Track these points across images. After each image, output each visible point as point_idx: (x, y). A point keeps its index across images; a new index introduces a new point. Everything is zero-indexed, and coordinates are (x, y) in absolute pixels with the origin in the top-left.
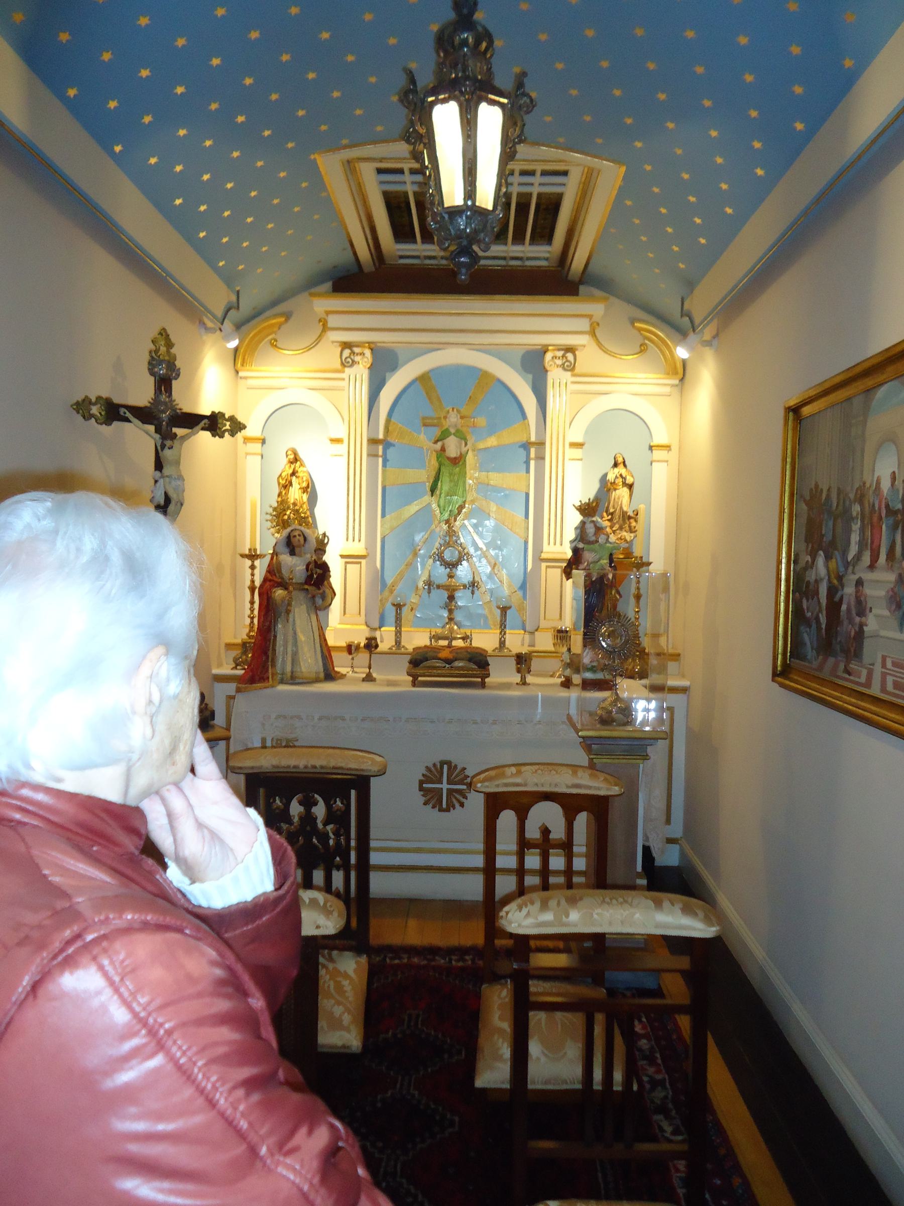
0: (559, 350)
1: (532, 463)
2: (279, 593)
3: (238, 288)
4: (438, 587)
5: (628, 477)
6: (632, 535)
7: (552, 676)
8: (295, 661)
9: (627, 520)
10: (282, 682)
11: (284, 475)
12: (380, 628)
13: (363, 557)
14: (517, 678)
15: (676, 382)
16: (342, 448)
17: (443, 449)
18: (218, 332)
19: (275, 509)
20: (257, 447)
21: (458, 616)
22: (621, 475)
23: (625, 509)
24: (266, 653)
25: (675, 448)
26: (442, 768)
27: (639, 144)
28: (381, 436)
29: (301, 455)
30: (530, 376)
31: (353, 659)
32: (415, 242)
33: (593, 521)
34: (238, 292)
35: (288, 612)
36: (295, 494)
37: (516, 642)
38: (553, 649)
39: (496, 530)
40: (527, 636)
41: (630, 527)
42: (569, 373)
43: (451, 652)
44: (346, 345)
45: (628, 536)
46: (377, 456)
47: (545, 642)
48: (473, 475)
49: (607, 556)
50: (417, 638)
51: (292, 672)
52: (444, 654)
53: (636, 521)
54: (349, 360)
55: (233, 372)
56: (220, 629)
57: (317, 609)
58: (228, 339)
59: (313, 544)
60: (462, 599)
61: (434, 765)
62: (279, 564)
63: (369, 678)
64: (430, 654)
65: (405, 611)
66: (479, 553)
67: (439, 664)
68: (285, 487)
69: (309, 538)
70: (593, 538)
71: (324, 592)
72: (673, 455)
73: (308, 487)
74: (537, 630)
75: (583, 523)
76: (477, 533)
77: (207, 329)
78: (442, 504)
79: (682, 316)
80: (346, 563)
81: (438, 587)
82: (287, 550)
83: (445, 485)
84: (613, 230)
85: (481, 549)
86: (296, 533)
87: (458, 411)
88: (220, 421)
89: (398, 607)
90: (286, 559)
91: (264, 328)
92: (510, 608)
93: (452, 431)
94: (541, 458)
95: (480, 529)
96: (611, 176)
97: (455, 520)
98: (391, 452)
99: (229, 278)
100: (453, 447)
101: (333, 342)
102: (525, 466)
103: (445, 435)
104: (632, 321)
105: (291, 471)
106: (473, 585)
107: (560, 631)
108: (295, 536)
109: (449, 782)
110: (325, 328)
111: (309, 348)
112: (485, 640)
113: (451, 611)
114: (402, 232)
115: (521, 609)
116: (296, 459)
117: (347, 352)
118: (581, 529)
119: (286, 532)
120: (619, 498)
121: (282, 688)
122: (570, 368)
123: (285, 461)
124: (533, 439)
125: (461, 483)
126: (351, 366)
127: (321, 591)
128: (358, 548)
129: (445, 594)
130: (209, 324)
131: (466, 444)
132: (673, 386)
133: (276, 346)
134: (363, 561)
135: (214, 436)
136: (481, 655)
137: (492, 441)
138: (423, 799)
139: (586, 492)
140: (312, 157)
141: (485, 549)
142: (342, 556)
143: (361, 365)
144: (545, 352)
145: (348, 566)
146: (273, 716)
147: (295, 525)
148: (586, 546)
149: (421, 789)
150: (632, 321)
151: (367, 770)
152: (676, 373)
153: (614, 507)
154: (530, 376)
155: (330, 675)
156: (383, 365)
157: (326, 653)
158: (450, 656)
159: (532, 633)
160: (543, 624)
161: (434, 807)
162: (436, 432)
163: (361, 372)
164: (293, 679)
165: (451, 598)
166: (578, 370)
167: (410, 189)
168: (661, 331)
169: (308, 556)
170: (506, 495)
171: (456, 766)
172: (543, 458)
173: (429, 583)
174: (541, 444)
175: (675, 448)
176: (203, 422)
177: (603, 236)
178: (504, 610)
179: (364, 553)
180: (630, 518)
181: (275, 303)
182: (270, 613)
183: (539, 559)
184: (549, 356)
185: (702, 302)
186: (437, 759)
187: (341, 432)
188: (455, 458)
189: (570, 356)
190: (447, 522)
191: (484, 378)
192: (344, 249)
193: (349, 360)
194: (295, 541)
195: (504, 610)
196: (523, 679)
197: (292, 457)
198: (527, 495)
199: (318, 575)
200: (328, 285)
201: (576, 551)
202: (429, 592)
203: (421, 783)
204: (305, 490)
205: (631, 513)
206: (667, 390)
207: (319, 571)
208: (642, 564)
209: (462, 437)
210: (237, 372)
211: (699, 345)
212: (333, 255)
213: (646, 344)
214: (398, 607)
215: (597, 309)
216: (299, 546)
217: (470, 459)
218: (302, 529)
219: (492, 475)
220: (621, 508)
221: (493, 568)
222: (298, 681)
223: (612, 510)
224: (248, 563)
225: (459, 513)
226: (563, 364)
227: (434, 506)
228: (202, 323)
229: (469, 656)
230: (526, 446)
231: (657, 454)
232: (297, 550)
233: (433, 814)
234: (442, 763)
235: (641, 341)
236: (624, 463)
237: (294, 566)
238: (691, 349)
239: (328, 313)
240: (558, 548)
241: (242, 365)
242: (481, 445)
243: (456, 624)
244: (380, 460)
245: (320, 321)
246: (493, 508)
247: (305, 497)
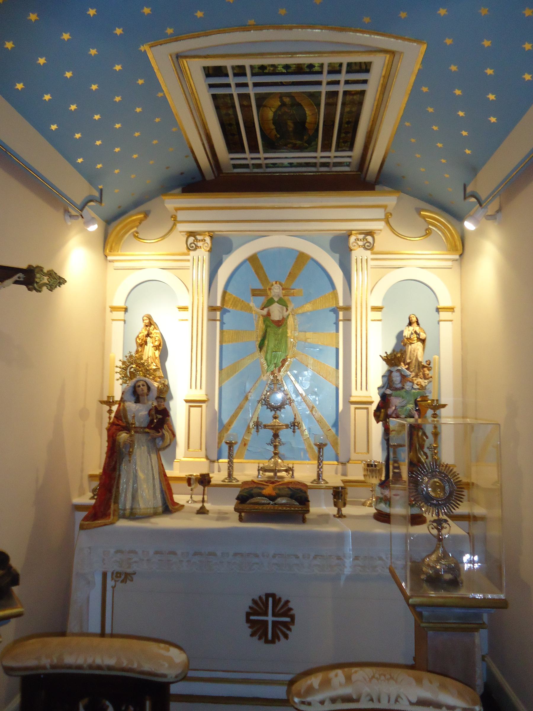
0: (361, 234)
1: (341, 324)
2: (123, 436)
3: (100, 187)
4: (265, 426)
5: (422, 334)
6: (426, 381)
7: (364, 504)
8: (134, 498)
9: (422, 368)
10: (124, 517)
11: (140, 335)
12: (218, 460)
13: (203, 402)
14: (334, 510)
15: (457, 257)
16: (187, 315)
17: (269, 314)
18: (80, 218)
19: (124, 363)
20: (121, 315)
21: (281, 450)
22: (416, 332)
23: (420, 359)
24: (110, 491)
25: (457, 310)
26: (267, 600)
27: (442, 12)
28: (219, 304)
29: (155, 319)
30: (338, 255)
31: (192, 490)
32: (244, 152)
33: (398, 371)
34: (101, 190)
35: (130, 454)
36: (149, 352)
37: (333, 477)
38: (362, 478)
39: (313, 379)
40: (340, 467)
41: (424, 374)
42: (369, 252)
43: (274, 489)
44: (191, 234)
45: (424, 382)
46: (215, 320)
47: (357, 473)
48: (292, 331)
49: (413, 401)
50: (248, 471)
51: (132, 509)
52: (269, 490)
53: (429, 370)
54: (193, 245)
55: (103, 257)
56: (82, 463)
57: (158, 450)
58: (88, 223)
59: (154, 394)
60: (285, 435)
61: (260, 598)
62: (124, 409)
63: (202, 511)
64: (255, 491)
65: (236, 448)
66: (300, 398)
67: (265, 501)
68: (141, 345)
69: (152, 388)
70: (399, 386)
71: (163, 434)
72: (456, 316)
73: (160, 345)
74: (348, 462)
75: (390, 372)
76: (298, 382)
77: (71, 216)
78: (269, 357)
79: (465, 198)
80: (191, 406)
81: (265, 426)
82: (133, 399)
83: (271, 343)
84: (407, 124)
85: (301, 395)
86: (140, 383)
87: (280, 284)
88: (38, 275)
89: (231, 445)
90: (131, 406)
91: (129, 223)
92: (325, 445)
93: (276, 299)
94: (348, 320)
95: (300, 378)
96: (413, 55)
97: (279, 371)
98: (226, 317)
99: (92, 178)
100: (276, 312)
101: (181, 232)
102: (334, 326)
103: (270, 302)
104: (418, 211)
105: (146, 333)
106: (295, 425)
107: (369, 465)
108: (139, 386)
109: (274, 615)
110: (175, 221)
111: (163, 237)
112: (304, 472)
113: (275, 447)
114: (234, 144)
115: (335, 444)
116: (150, 323)
117: (191, 239)
118: (388, 378)
119: (131, 383)
120: (414, 351)
121: (122, 523)
122: (369, 247)
123: (142, 325)
124: (341, 304)
125: (283, 341)
126: (195, 249)
127: (160, 434)
128: (200, 394)
129: (271, 433)
130: (74, 213)
131: (287, 310)
132: (453, 260)
133: (137, 237)
134: (204, 405)
135: (29, 289)
136: (301, 490)
137: (308, 307)
138: (250, 631)
139: (389, 346)
140: (142, 48)
141: (304, 395)
142: (187, 401)
143: (203, 249)
144: (349, 236)
145: (191, 408)
146: (112, 551)
147: (140, 376)
148: (394, 393)
149: (248, 620)
150: (418, 211)
151: (165, 676)
152: (457, 250)
153: (410, 359)
154: (338, 255)
155: (169, 507)
156: (220, 249)
157: (166, 485)
158: (274, 493)
159: (343, 464)
160: (353, 456)
161: (260, 639)
162: (262, 300)
163: (203, 254)
164: (133, 516)
165: (276, 436)
166: (376, 249)
167: (234, 91)
168: (443, 217)
169: (150, 403)
170: (320, 350)
171: (280, 599)
172: (350, 320)
173: (257, 425)
174: (347, 309)
175: (457, 310)
176: (18, 275)
177: (400, 131)
178: (321, 446)
179: (204, 398)
180: (424, 367)
181: (137, 204)
182: (115, 455)
183: (348, 402)
184: (352, 239)
185: (486, 182)
186: (262, 593)
187: (186, 301)
188: (279, 321)
189: (369, 238)
190: (273, 373)
191: (302, 259)
192: (187, 157)
193: (193, 245)
194: (139, 390)
195: (321, 446)
196: (339, 510)
197: (147, 321)
198: (337, 350)
199: (160, 419)
200: (179, 190)
201: (384, 398)
202: (258, 431)
203: (248, 615)
204: (157, 348)
205: (424, 363)
206: (449, 263)
207: (160, 416)
208: (438, 406)
209: (282, 302)
210: (106, 257)
211: (484, 219)
212: (180, 164)
213: (430, 229)
214: (231, 445)
215: (390, 200)
216: (143, 395)
217: (290, 321)
218: (146, 379)
219: (308, 335)
220: (417, 359)
221: (311, 411)
222: (137, 516)
223: (408, 361)
224: (107, 408)
225: (282, 366)
226: (364, 245)
227: (263, 360)
228: (66, 211)
229: (290, 492)
230: (335, 310)
231: (443, 315)
232: (141, 398)
233: (257, 644)
234: (268, 595)
235: (426, 227)
236: (417, 322)
237: (139, 412)
238: (476, 222)
239: (177, 209)
240: (364, 393)
241: (110, 251)
242: (300, 311)
243: (280, 458)
244: (218, 323)
245: (172, 217)
246: (311, 361)
247: (157, 353)
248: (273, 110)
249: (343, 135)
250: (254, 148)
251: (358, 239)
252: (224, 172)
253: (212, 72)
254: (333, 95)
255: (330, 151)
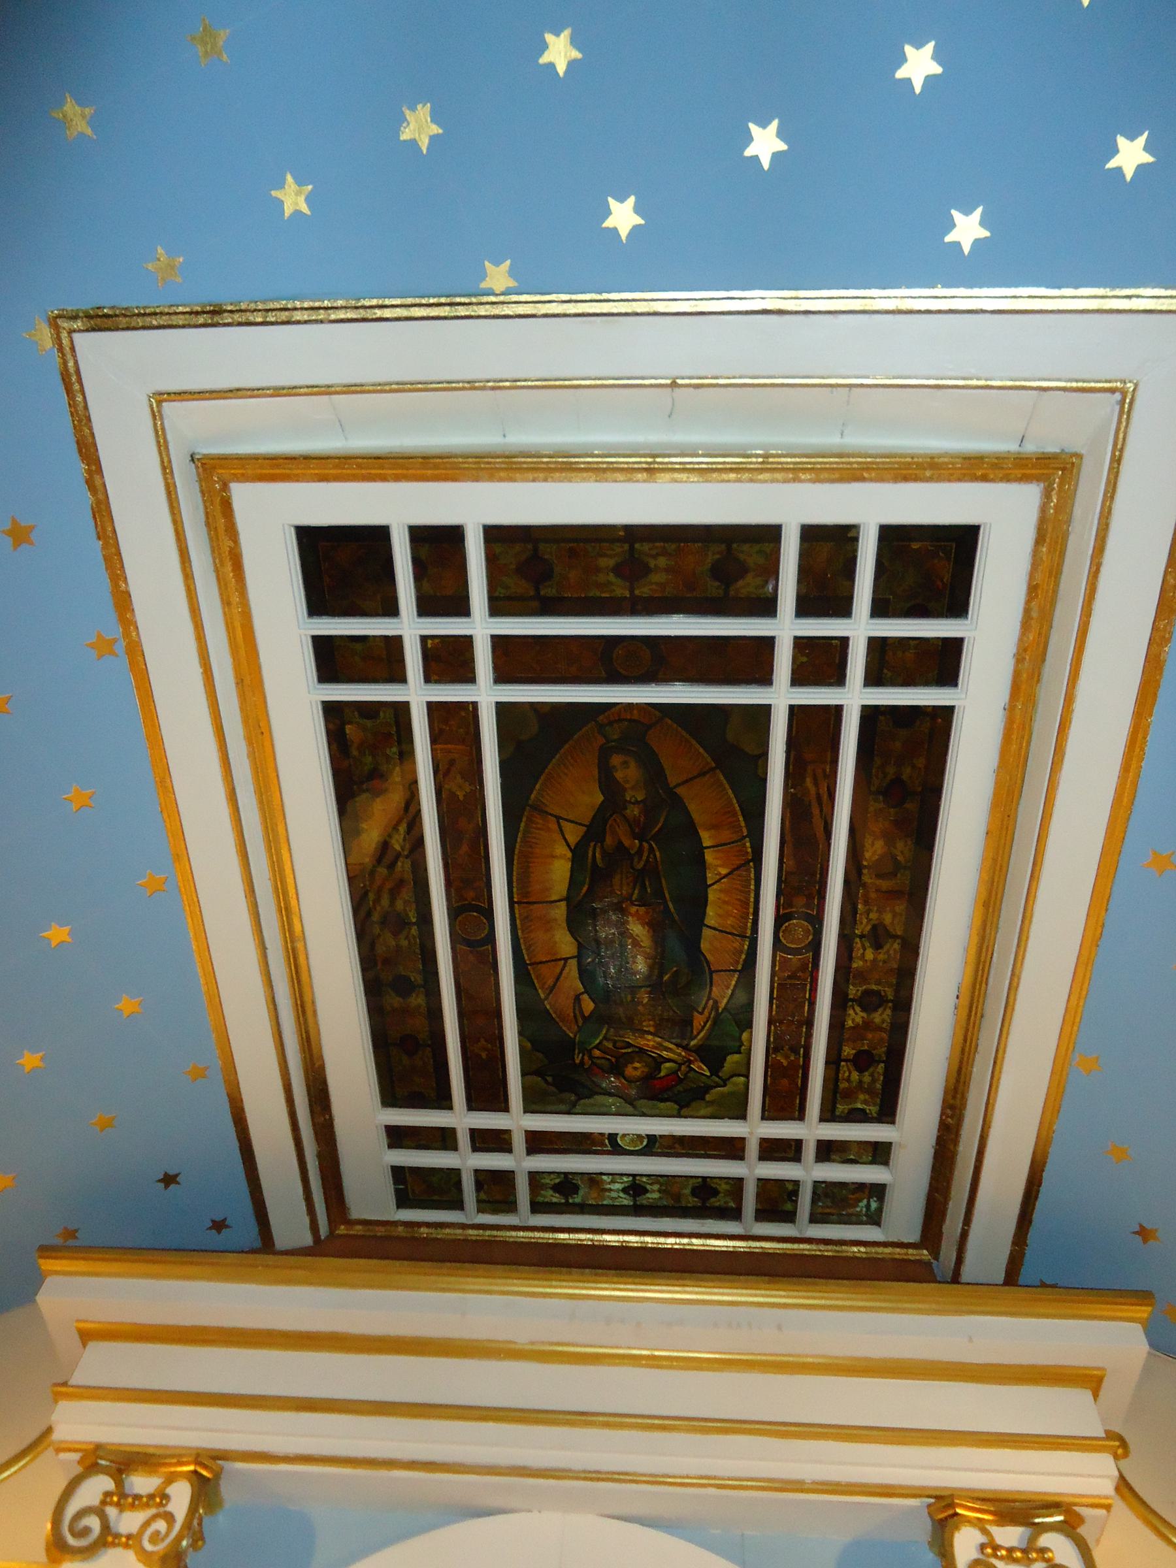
32: (443, 1101)
114: (406, 1064)
193: (94, 1522)
248: (574, 834)
249: (855, 1016)
250: (487, 1091)
251: (996, 1548)
252: (355, 1214)
253: (341, 566)
254: (785, 1100)
255: (801, 1117)
